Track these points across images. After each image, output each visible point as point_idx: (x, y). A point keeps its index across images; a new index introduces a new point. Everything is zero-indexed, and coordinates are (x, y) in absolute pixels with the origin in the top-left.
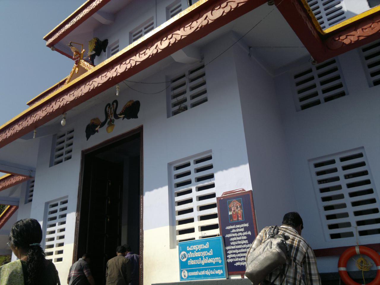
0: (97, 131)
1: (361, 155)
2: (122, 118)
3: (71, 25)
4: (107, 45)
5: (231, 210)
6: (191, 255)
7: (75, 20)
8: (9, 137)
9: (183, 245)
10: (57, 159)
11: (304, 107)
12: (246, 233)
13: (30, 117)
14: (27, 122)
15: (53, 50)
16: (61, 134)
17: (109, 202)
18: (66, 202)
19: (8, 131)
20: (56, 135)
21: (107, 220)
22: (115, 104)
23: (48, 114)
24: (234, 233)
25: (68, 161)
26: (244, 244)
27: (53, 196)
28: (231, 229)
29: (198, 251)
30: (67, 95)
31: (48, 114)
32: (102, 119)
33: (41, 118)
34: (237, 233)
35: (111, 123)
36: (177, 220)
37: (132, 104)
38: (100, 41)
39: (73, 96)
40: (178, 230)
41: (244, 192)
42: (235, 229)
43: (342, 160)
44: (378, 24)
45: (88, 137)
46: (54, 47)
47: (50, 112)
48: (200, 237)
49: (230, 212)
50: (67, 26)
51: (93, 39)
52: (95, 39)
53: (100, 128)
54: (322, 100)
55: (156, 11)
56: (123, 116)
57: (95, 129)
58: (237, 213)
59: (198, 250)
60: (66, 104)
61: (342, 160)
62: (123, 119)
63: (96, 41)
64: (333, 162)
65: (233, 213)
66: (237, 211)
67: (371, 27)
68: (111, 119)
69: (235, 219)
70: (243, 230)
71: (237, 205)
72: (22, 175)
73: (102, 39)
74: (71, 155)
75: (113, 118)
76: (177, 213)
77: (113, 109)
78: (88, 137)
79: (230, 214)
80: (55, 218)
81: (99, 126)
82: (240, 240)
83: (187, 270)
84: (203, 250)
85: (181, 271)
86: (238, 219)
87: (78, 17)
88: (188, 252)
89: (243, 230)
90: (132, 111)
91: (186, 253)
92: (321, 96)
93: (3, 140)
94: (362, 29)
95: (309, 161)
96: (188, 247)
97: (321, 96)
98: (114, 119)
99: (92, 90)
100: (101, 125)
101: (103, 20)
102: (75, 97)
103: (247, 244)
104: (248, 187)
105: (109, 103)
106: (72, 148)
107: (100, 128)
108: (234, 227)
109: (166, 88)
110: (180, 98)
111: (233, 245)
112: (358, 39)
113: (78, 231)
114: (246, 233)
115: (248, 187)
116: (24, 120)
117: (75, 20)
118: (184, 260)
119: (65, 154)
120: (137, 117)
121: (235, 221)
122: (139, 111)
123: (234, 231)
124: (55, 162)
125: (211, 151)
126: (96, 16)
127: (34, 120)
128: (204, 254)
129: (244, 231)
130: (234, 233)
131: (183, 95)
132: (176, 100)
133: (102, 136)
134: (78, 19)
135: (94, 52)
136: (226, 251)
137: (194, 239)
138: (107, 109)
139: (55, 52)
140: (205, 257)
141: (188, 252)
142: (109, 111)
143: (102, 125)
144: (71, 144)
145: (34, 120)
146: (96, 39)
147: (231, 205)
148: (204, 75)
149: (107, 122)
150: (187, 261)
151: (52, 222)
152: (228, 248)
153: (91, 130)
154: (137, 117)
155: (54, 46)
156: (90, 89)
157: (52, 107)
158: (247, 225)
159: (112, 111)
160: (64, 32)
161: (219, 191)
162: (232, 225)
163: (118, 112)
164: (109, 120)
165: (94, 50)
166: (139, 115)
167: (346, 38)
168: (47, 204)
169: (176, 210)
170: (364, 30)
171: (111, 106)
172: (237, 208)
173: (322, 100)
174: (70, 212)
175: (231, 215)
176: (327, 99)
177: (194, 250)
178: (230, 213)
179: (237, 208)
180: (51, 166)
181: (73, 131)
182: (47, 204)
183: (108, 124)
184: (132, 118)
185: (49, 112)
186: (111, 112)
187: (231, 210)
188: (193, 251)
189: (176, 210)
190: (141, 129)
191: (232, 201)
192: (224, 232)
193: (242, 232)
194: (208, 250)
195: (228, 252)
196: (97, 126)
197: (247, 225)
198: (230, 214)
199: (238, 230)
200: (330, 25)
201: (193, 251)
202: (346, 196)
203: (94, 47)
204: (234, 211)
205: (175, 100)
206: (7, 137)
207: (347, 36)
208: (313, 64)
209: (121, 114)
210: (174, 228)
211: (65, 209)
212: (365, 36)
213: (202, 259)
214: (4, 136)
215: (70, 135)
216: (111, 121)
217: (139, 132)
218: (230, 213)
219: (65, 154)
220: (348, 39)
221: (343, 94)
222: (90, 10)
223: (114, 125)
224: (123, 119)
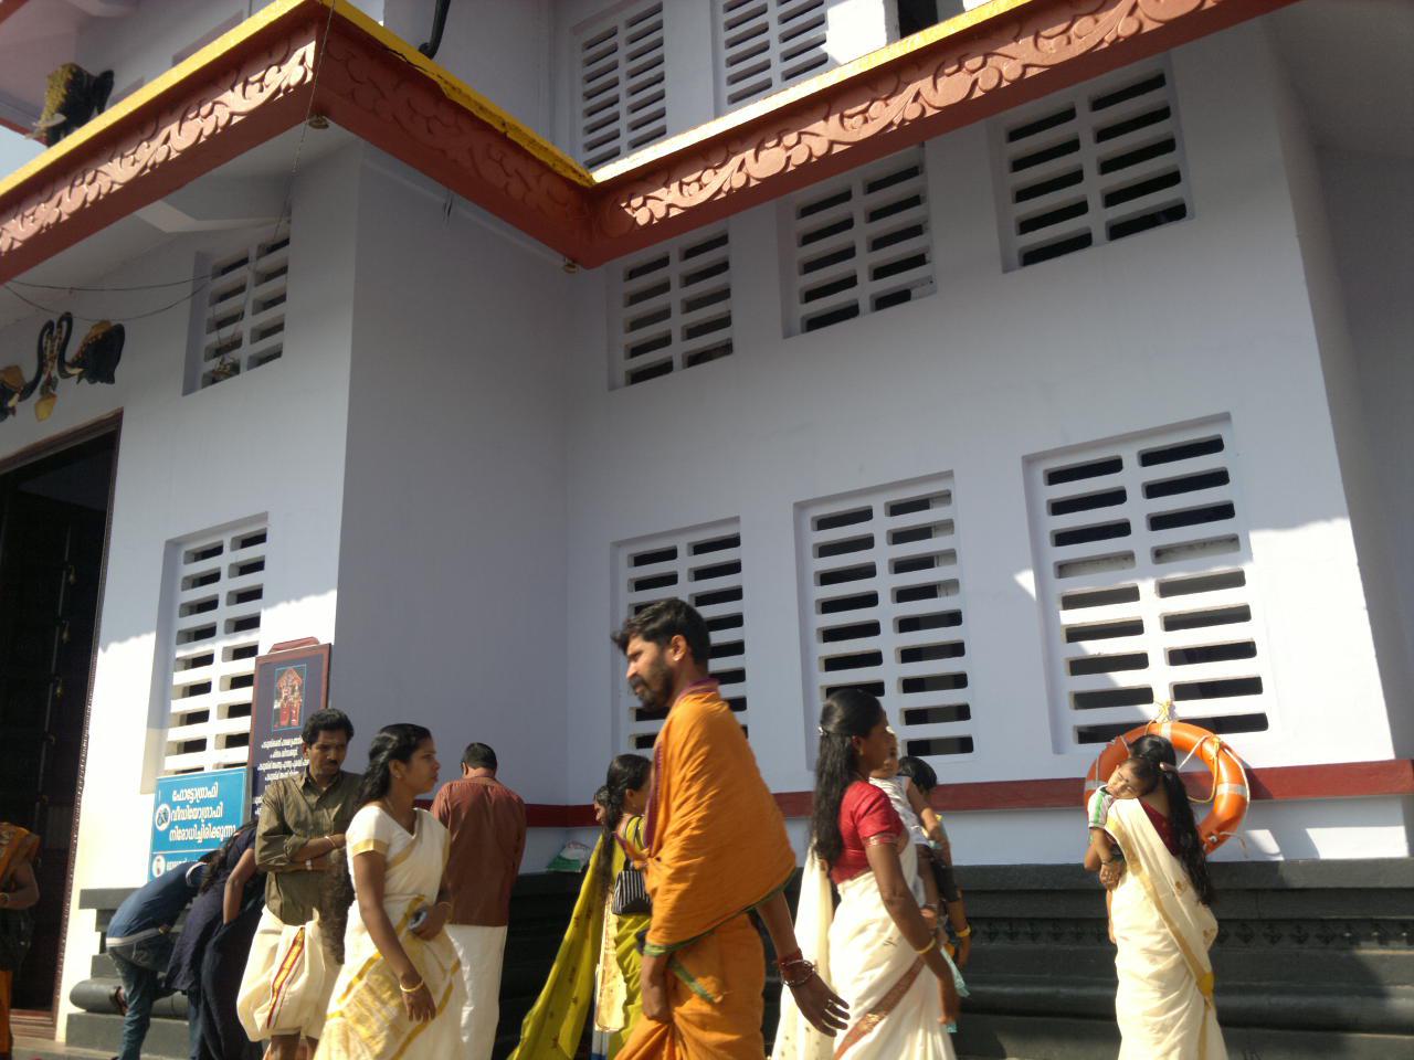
0: (13, 410)
1: (733, 542)
2: (75, 378)
5: (279, 697)
6: (179, 814)
9: (165, 791)
11: (1032, 257)
12: (298, 763)
13: (68, 188)
17: (65, 636)
22: (65, 324)
24: (276, 760)
25: (260, 368)
28: (272, 750)
29: (195, 805)
30: (233, 90)
31: (148, 171)
32: (29, 374)
33: (17, 245)
34: (283, 760)
35: (47, 391)
36: (175, 714)
37: (104, 334)
40: (174, 742)
42: (280, 749)
44: (887, 105)
47: (154, 164)
49: (276, 702)
53: (20, 400)
56: (76, 371)
57: (6, 403)
58: (290, 707)
59: (195, 801)
60: (108, 195)
61: (1148, 459)
64: (671, 554)
65: (282, 705)
66: (291, 699)
67: (699, 180)
69: (284, 723)
70: (294, 753)
71: (295, 682)
75: (55, 373)
77: (57, 341)
79: (275, 707)
80: (207, 633)
81: (17, 396)
83: (165, 856)
84: (204, 803)
85: (153, 857)
86: (290, 724)
88: (173, 806)
89: (294, 753)
90: (102, 356)
91: (168, 809)
93: (44, 231)
95: (619, 545)
96: (175, 792)
97: (1096, 220)
98: (58, 377)
99: (208, 137)
102: (138, 167)
104: (327, 636)
105: (52, 318)
107: (20, 400)
109: (193, 294)
110: (227, 332)
112: (668, 213)
114: (298, 763)
115: (327, 636)
116: (146, 137)
118: (164, 827)
119: (252, 342)
120: (110, 379)
121: (284, 727)
122: (119, 359)
123: (276, 754)
127: (86, 196)
128: (206, 812)
130: (276, 760)
132: (216, 339)
137: (202, 769)
138: (44, 340)
140: (207, 821)
141: (173, 806)
142: (48, 350)
143: (27, 391)
145: (86, 196)
147: (283, 683)
149: (39, 387)
150: (168, 831)
151: (200, 648)
154: (110, 379)
156: (201, 133)
157: (167, 139)
159: (55, 348)
161: (265, 638)
162: (276, 737)
163: (70, 355)
164: (44, 378)
166: (119, 372)
167: (799, 142)
169: (175, 683)
171: (55, 333)
172: (293, 691)
174: (273, 604)
175: (278, 710)
176: (1118, 231)
177: (187, 802)
178: (277, 705)
179: (293, 691)
180: (189, 389)
181: (286, 242)
183: (42, 393)
184: (102, 382)
185: (150, 164)
186: (52, 352)
187: (279, 697)
188: (183, 804)
189: (175, 683)
191: (284, 671)
193: (292, 759)
194: (212, 803)
196: (11, 395)
198: (275, 707)
199: (285, 753)
201: (183, 804)
202: (1153, 625)
204: (286, 698)
205: (213, 339)
207: (646, 199)
209: (73, 365)
211: (254, 594)
212: (683, 209)
213: (199, 829)
214: (19, 229)
216: (51, 383)
217: (110, 430)
218: (277, 705)
219: (252, 342)
220: (643, 212)
221: (1176, 213)
223: (54, 396)
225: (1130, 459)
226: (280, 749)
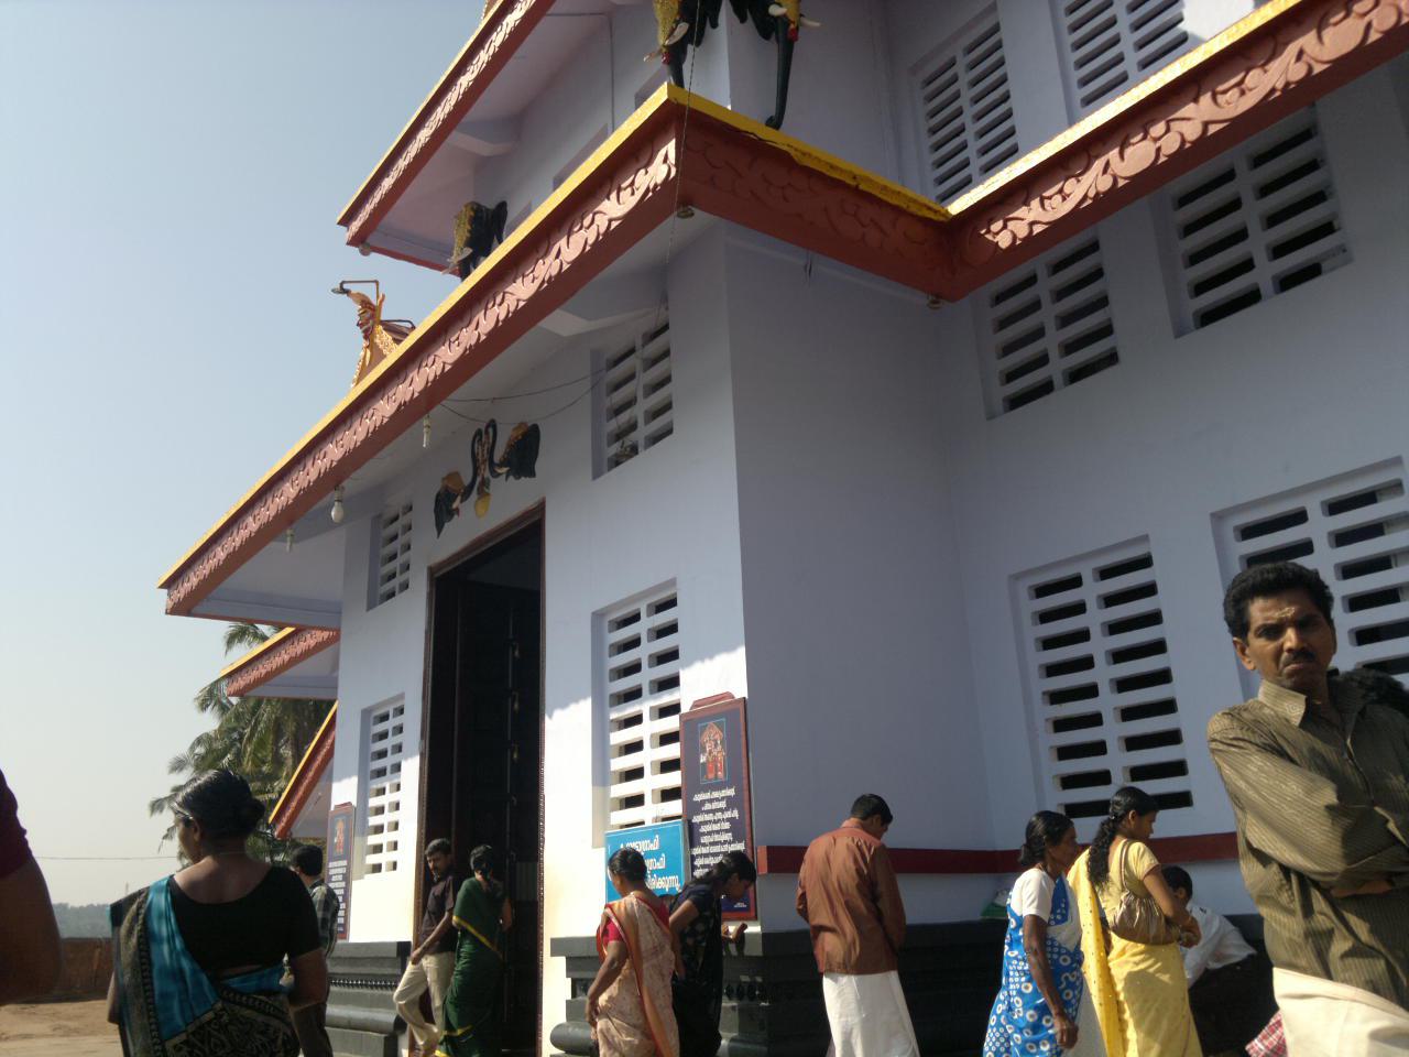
0: (457, 510)
1: (1145, 562)
2: (504, 476)
3: (523, 12)
4: (504, 222)
5: (704, 750)
7: (402, 163)
8: (490, 334)
10: (383, 591)
12: (728, 815)
13: (565, 239)
14: (476, 329)
15: (364, 253)
16: (389, 514)
18: (671, 603)
19: (358, 422)
20: (380, 516)
21: (512, 756)
22: (491, 430)
23: (650, 194)
24: (708, 812)
25: (389, 601)
26: (725, 842)
27: (626, 583)
28: (703, 802)
31: (546, 285)
36: (614, 772)
38: (487, 210)
39: (633, 194)
41: (730, 703)
42: (711, 801)
43: (1335, 507)
45: (440, 526)
46: (368, 245)
47: (550, 277)
48: (656, 820)
50: (388, 183)
51: (464, 209)
52: (469, 207)
53: (462, 501)
54: (1266, 287)
55: (613, 106)
56: (505, 470)
58: (715, 760)
61: (1335, 507)
62: (507, 479)
63: (472, 214)
64: (1299, 517)
65: (708, 760)
66: (715, 753)
68: (483, 478)
69: (711, 776)
70: (723, 805)
71: (717, 736)
72: (323, 629)
73: (490, 204)
74: (671, 422)
75: (487, 474)
76: (617, 751)
78: (440, 526)
79: (702, 761)
81: (459, 498)
82: (718, 832)
87: (448, 105)
89: (723, 805)
90: (523, 455)
92: (1265, 273)
94: (1214, 98)
95: (1017, 577)
98: (491, 478)
100: (464, 493)
101: (484, 148)
103: (730, 843)
104: (740, 690)
106: (670, 396)
107: (462, 501)
108: (706, 796)
111: (704, 845)
113: (425, 789)
114: (728, 815)
115: (740, 690)
116: (466, 324)
117: (402, 163)
120: (532, 474)
121: (710, 780)
123: (707, 807)
124: (382, 596)
125: (672, 583)
126: (456, 138)
129: (727, 809)
131: (629, 411)
133: (474, 523)
134: (447, 110)
135: (468, 251)
136: (693, 858)
137: (643, 823)
138: (476, 445)
139: (374, 255)
144: (666, 380)
146: (472, 209)
147: (705, 738)
148: (666, 354)
152: (696, 851)
153: (444, 510)
154: (532, 474)
155: (368, 241)
158: (731, 792)
160: (503, 45)
164: (479, 479)
165: (469, 243)
166: (539, 466)
168: (598, 616)
170: (1221, 99)
173: (1266, 287)
175: (703, 764)
178: (703, 759)
179: (716, 745)
182: (366, 713)
190: (540, 509)
192: (692, 808)
195: (696, 863)
197: (731, 792)
198: (702, 761)
200: (1145, 64)
203: (468, 235)
204: (710, 752)
205: (613, 425)
206: (483, 338)
208: (935, 308)
209: (501, 465)
210: (606, 793)
215: (654, 348)
216: (485, 483)
218: (703, 759)
222: (431, 131)
224: (507, 479)
225: (1313, 505)
226: (711, 801)
